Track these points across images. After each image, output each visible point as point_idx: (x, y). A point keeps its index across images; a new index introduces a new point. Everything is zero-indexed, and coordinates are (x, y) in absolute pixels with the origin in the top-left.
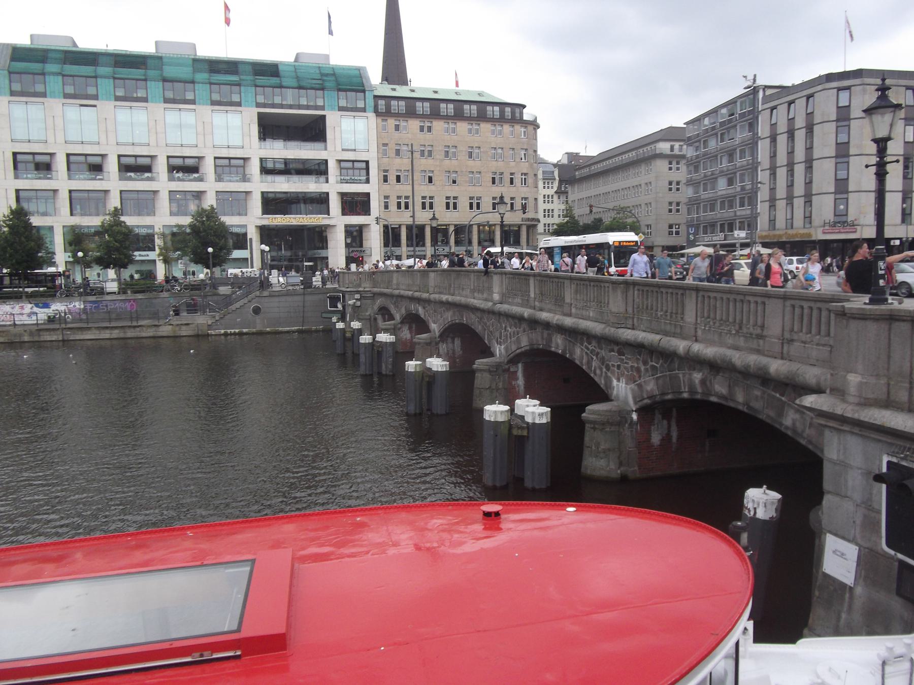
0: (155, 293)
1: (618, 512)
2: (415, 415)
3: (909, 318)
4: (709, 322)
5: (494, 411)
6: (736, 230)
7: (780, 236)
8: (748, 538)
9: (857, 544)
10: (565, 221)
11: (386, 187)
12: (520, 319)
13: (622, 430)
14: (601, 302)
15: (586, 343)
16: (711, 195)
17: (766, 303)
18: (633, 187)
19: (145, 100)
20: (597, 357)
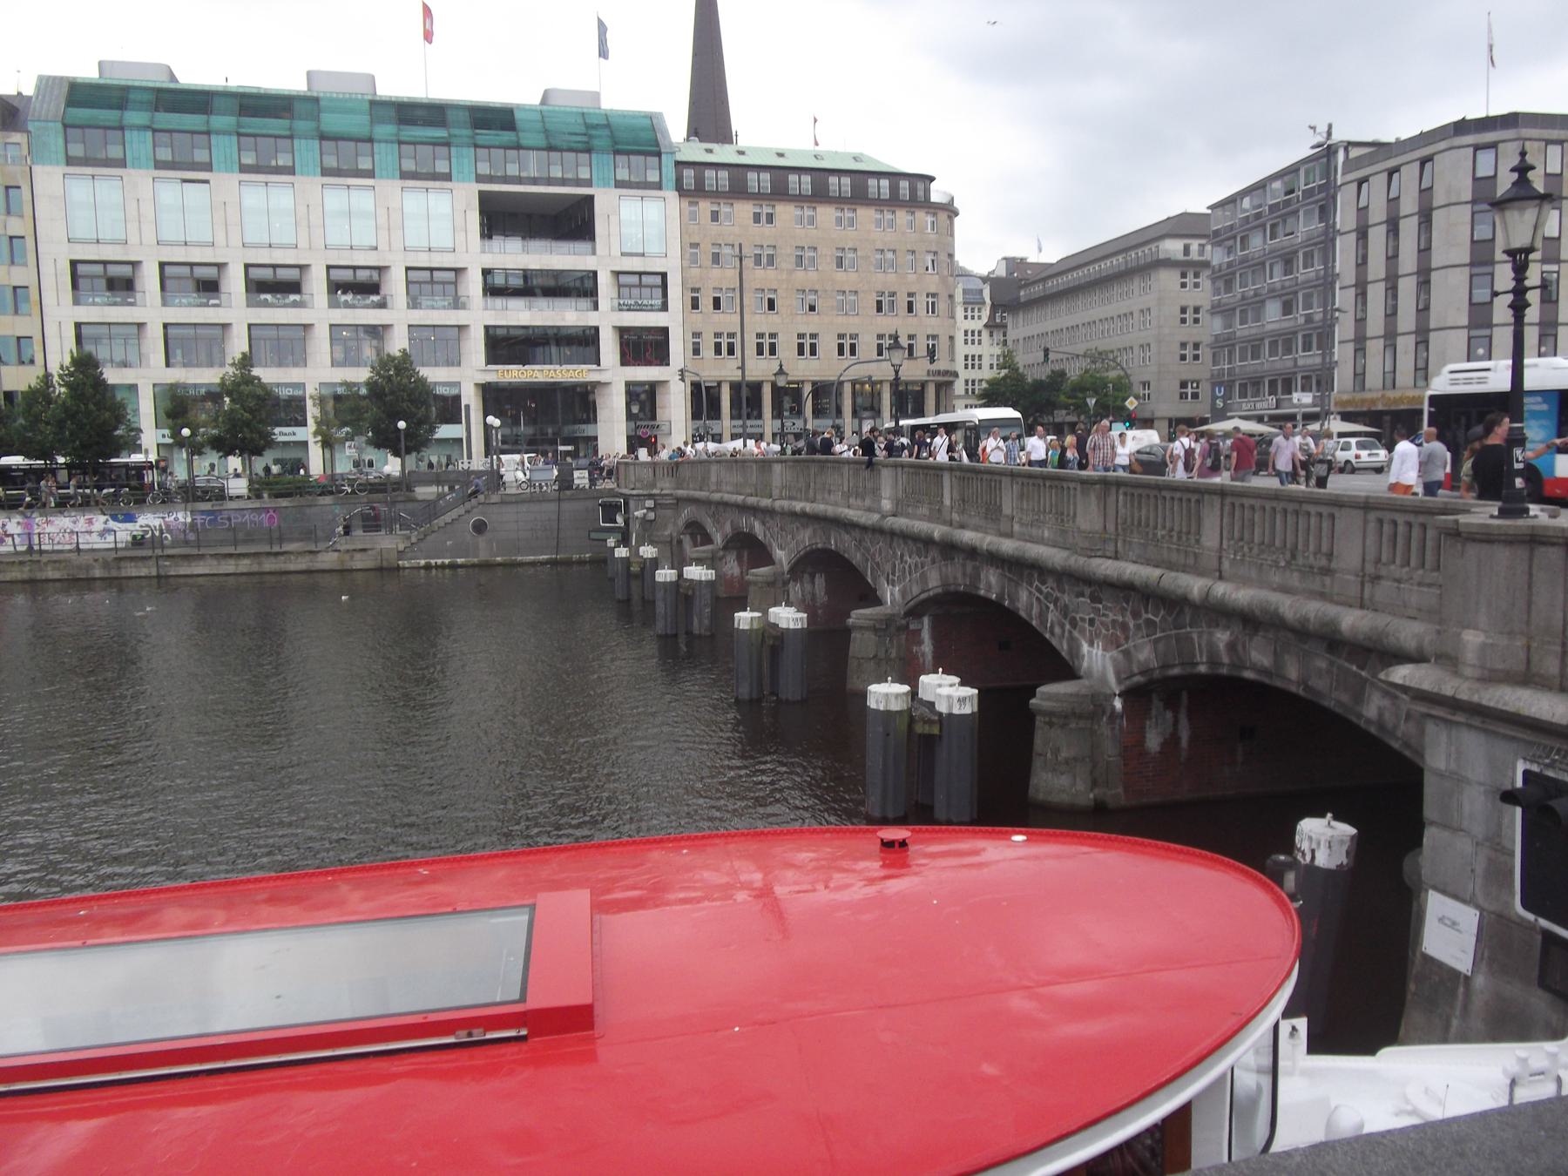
0: (310, 498)
1: (1094, 843)
2: (751, 701)
3: (1561, 541)
4: (1243, 547)
5: (885, 694)
6: (1296, 391)
7: (1373, 401)
8: (1297, 879)
9: (1477, 906)
10: (1002, 374)
11: (696, 316)
12: (926, 542)
13: (1096, 727)
14: (1062, 514)
15: (1036, 583)
16: (1253, 331)
17: (1337, 515)
18: (1119, 316)
19: (291, 171)
20: (1055, 605)
